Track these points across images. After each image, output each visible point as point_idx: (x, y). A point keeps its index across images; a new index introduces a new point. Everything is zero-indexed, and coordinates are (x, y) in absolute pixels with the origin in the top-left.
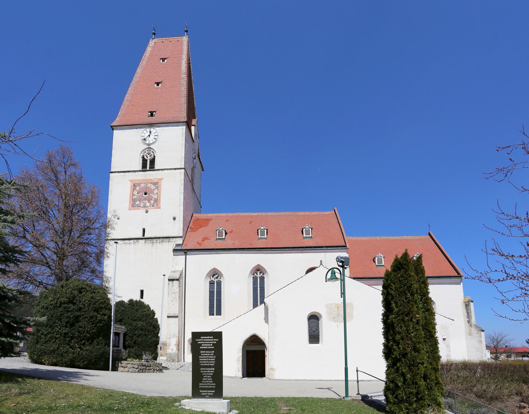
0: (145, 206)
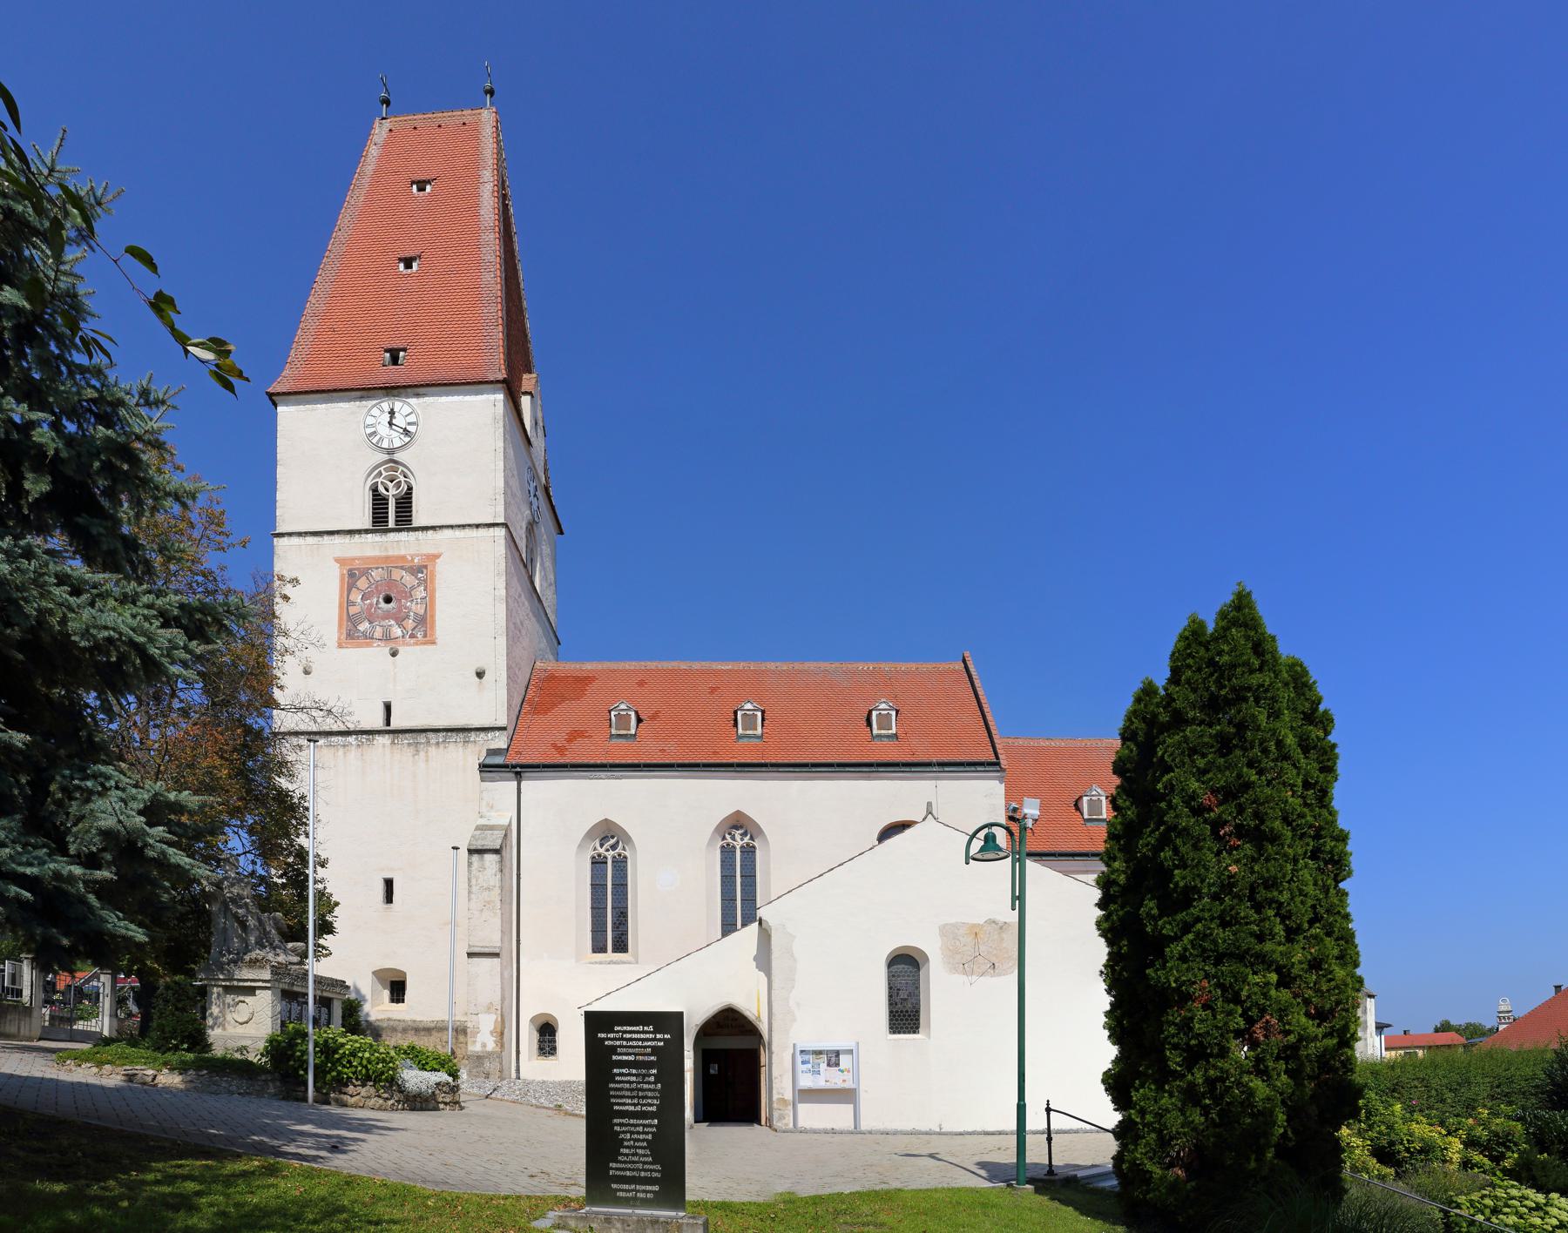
0: (387, 637)
